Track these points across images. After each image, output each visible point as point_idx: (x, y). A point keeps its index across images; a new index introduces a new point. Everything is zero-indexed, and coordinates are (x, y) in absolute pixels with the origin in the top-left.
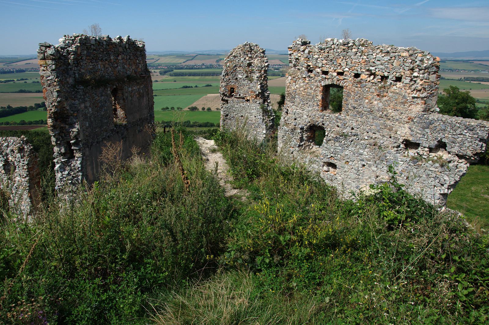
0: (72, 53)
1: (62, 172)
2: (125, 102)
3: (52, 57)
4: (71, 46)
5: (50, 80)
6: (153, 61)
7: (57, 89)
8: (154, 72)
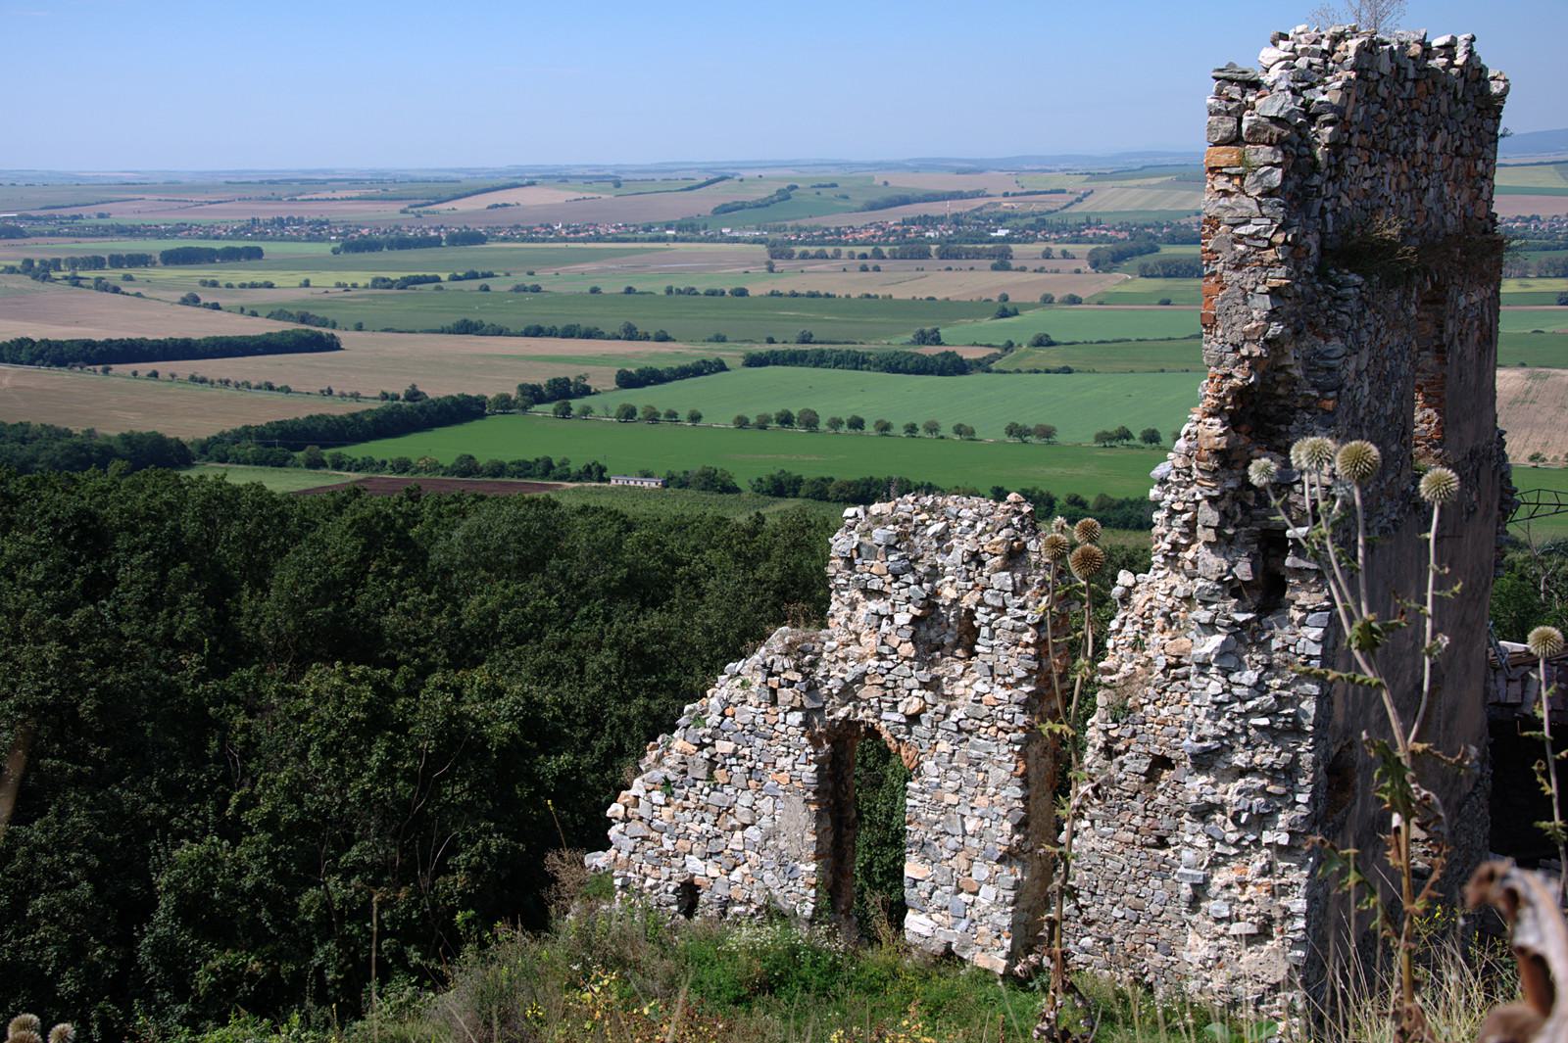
0: (1329, 116)
1: (1226, 672)
2: (1443, 362)
3: (1276, 129)
4: (1322, 82)
5: (1250, 236)
6: (1061, 200)
7: (1275, 283)
8: (1065, 254)
